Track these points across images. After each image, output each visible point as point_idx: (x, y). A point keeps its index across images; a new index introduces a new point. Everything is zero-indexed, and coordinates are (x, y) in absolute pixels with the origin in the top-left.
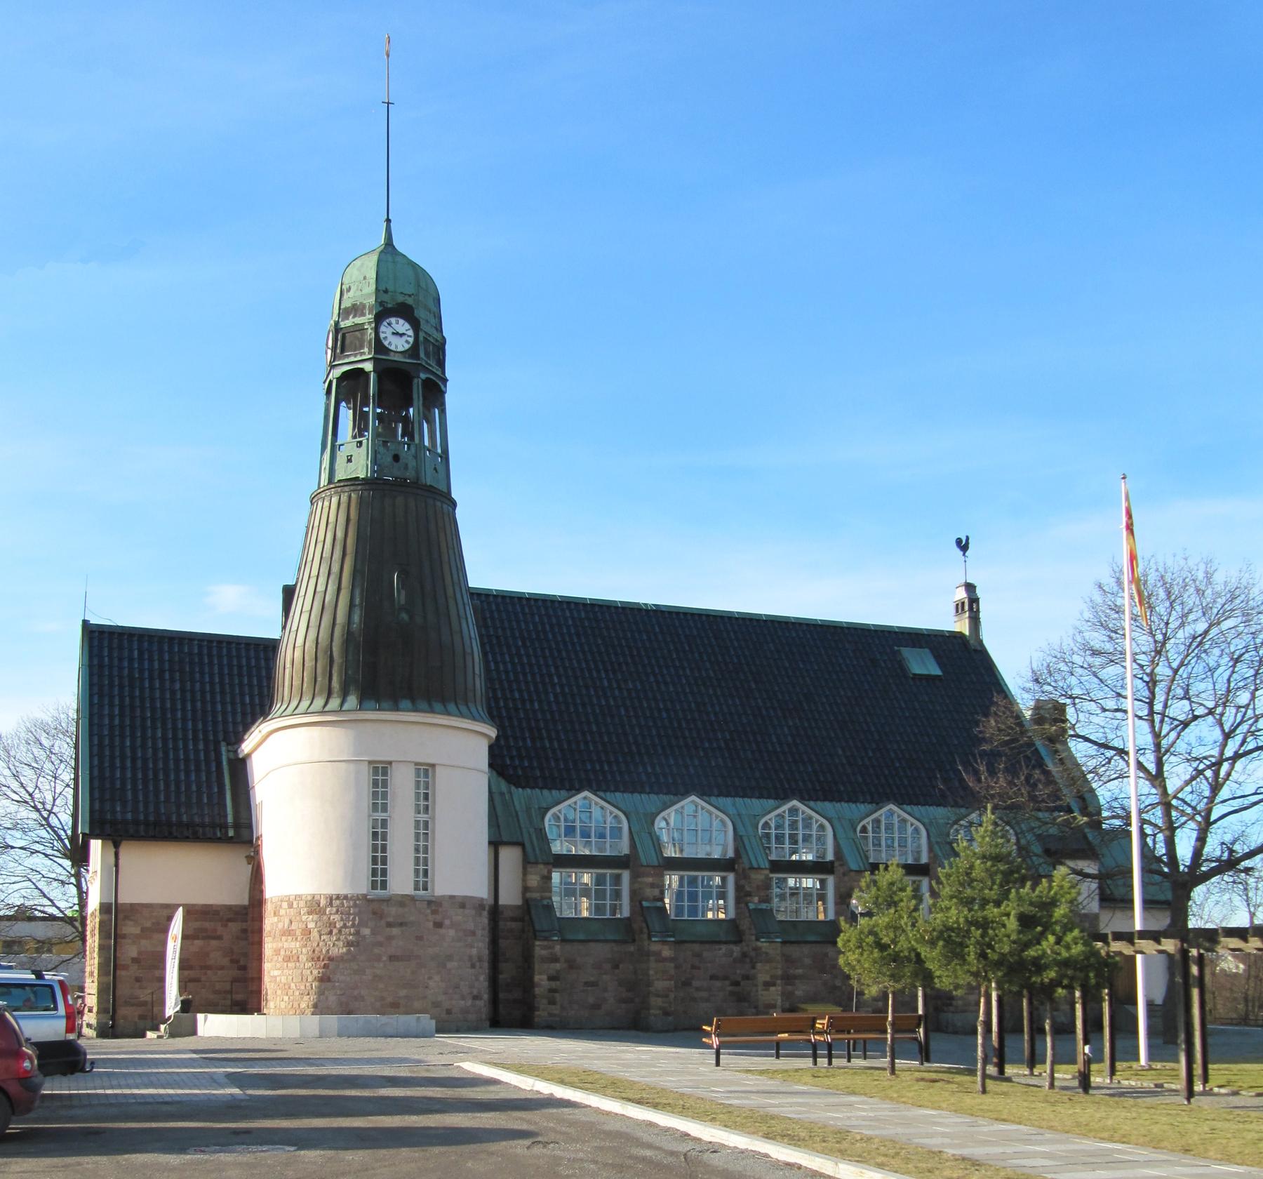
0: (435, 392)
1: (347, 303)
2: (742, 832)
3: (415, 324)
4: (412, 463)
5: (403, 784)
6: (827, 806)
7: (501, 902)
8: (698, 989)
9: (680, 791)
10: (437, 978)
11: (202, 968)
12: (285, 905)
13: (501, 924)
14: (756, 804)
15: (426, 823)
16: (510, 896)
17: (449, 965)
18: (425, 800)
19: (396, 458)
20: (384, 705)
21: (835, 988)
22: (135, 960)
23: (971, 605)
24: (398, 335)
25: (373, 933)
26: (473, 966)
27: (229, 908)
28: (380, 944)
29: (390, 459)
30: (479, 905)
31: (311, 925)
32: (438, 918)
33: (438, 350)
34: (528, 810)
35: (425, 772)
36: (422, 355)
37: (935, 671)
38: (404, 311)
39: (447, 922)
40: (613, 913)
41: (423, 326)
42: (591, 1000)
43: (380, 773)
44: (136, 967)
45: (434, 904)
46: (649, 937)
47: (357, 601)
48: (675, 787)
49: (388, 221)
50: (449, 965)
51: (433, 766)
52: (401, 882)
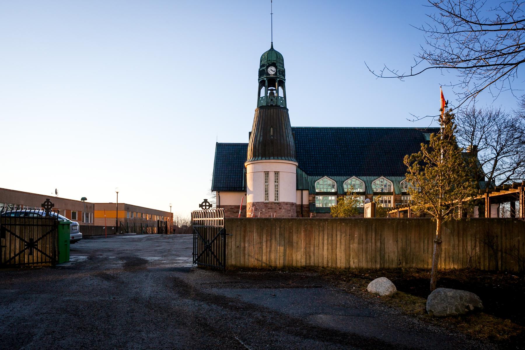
0: (282, 83)
3: (276, 67)
4: (275, 101)
5: (272, 176)
6: (393, 178)
9: (379, 175)
13: (303, 209)
14: (342, 178)
16: (306, 202)
18: (277, 181)
19: (272, 100)
21: (275, 212)
24: (271, 71)
30: (297, 206)
34: (311, 181)
35: (277, 173)
38: (274, 65)
41: (278, 67)
43: (267, 173)
48: (349, 174)
52: (501, 216)
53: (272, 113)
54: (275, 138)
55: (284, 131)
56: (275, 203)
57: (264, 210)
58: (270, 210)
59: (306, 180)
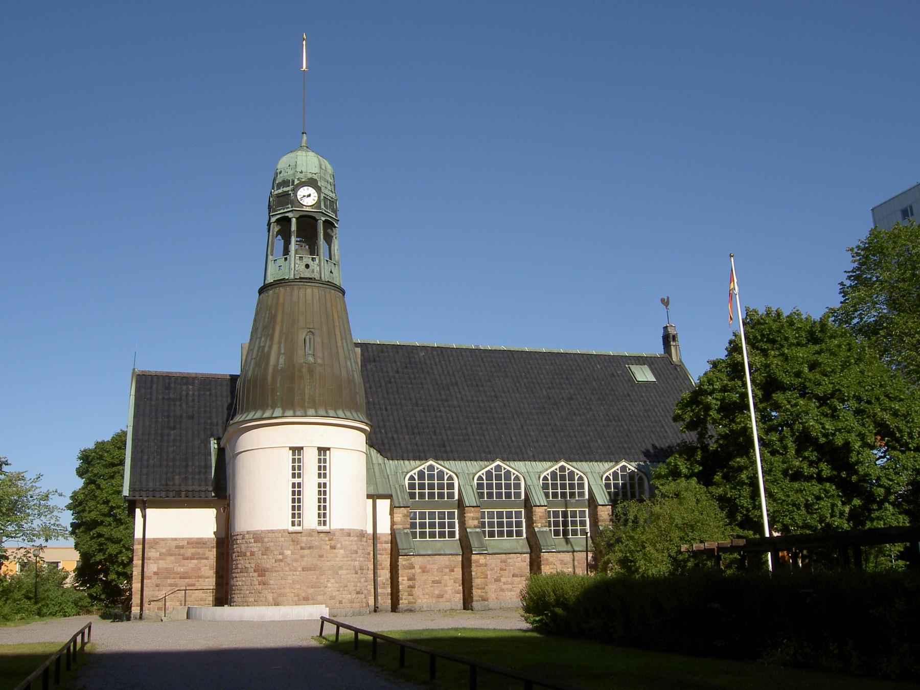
3: (318, 190)
5: (310, 460)
7: (378, 532)
8: (504, 583)
10: (332, 581)
11: (196, 577)
17: (340, 572)
22: (155, 573)
26: (356, 573)
28: (296, 560)
29: (303, 267)
30: (362, 534)
32: (333, 543)
36: (323, 206)
37: (652, 378)
39: (339, 545)
42: (437, 592)
43: (297, 450)
44: (156, 577)
50: (340, 572)
53: (309, 297)
54: (319, 361)
55: (339, 344)
57: (289, 552)
58: (306, 552)
59: (381, 471)
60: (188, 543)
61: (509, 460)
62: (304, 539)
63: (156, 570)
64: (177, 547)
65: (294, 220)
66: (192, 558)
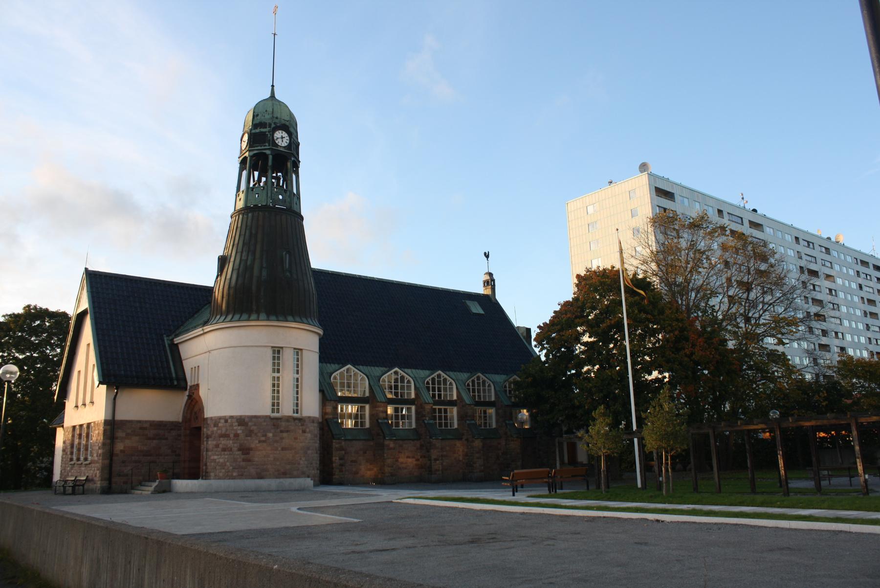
1: (257, 121)
2: (418, 385)
3: (290, 134)
12: (222, 421)
15: (278, 378)
20: (280, 318)
22: (122, 451)
23: (490, 282)
25: (274, 436)
27: (172, 423)
28: (276, 442)
31: (239, 432)
33: (297, 145)
37: (482, 312)
40: (362, 426)
42: (354, 469)
43: (277, 351)
45: (301, 420)
46: (384, 438)
47: (265, 265)
49: (273, 86)
51: (301, 350)
56: (295, 419)
57: (270, 435)
58: (285, 435)
60: (151, 425)
61: (358, 365)
62: (283, 424)
63: (122, 448)
64: (141, 428)
65: (270, 157)
66: (154, 439)
